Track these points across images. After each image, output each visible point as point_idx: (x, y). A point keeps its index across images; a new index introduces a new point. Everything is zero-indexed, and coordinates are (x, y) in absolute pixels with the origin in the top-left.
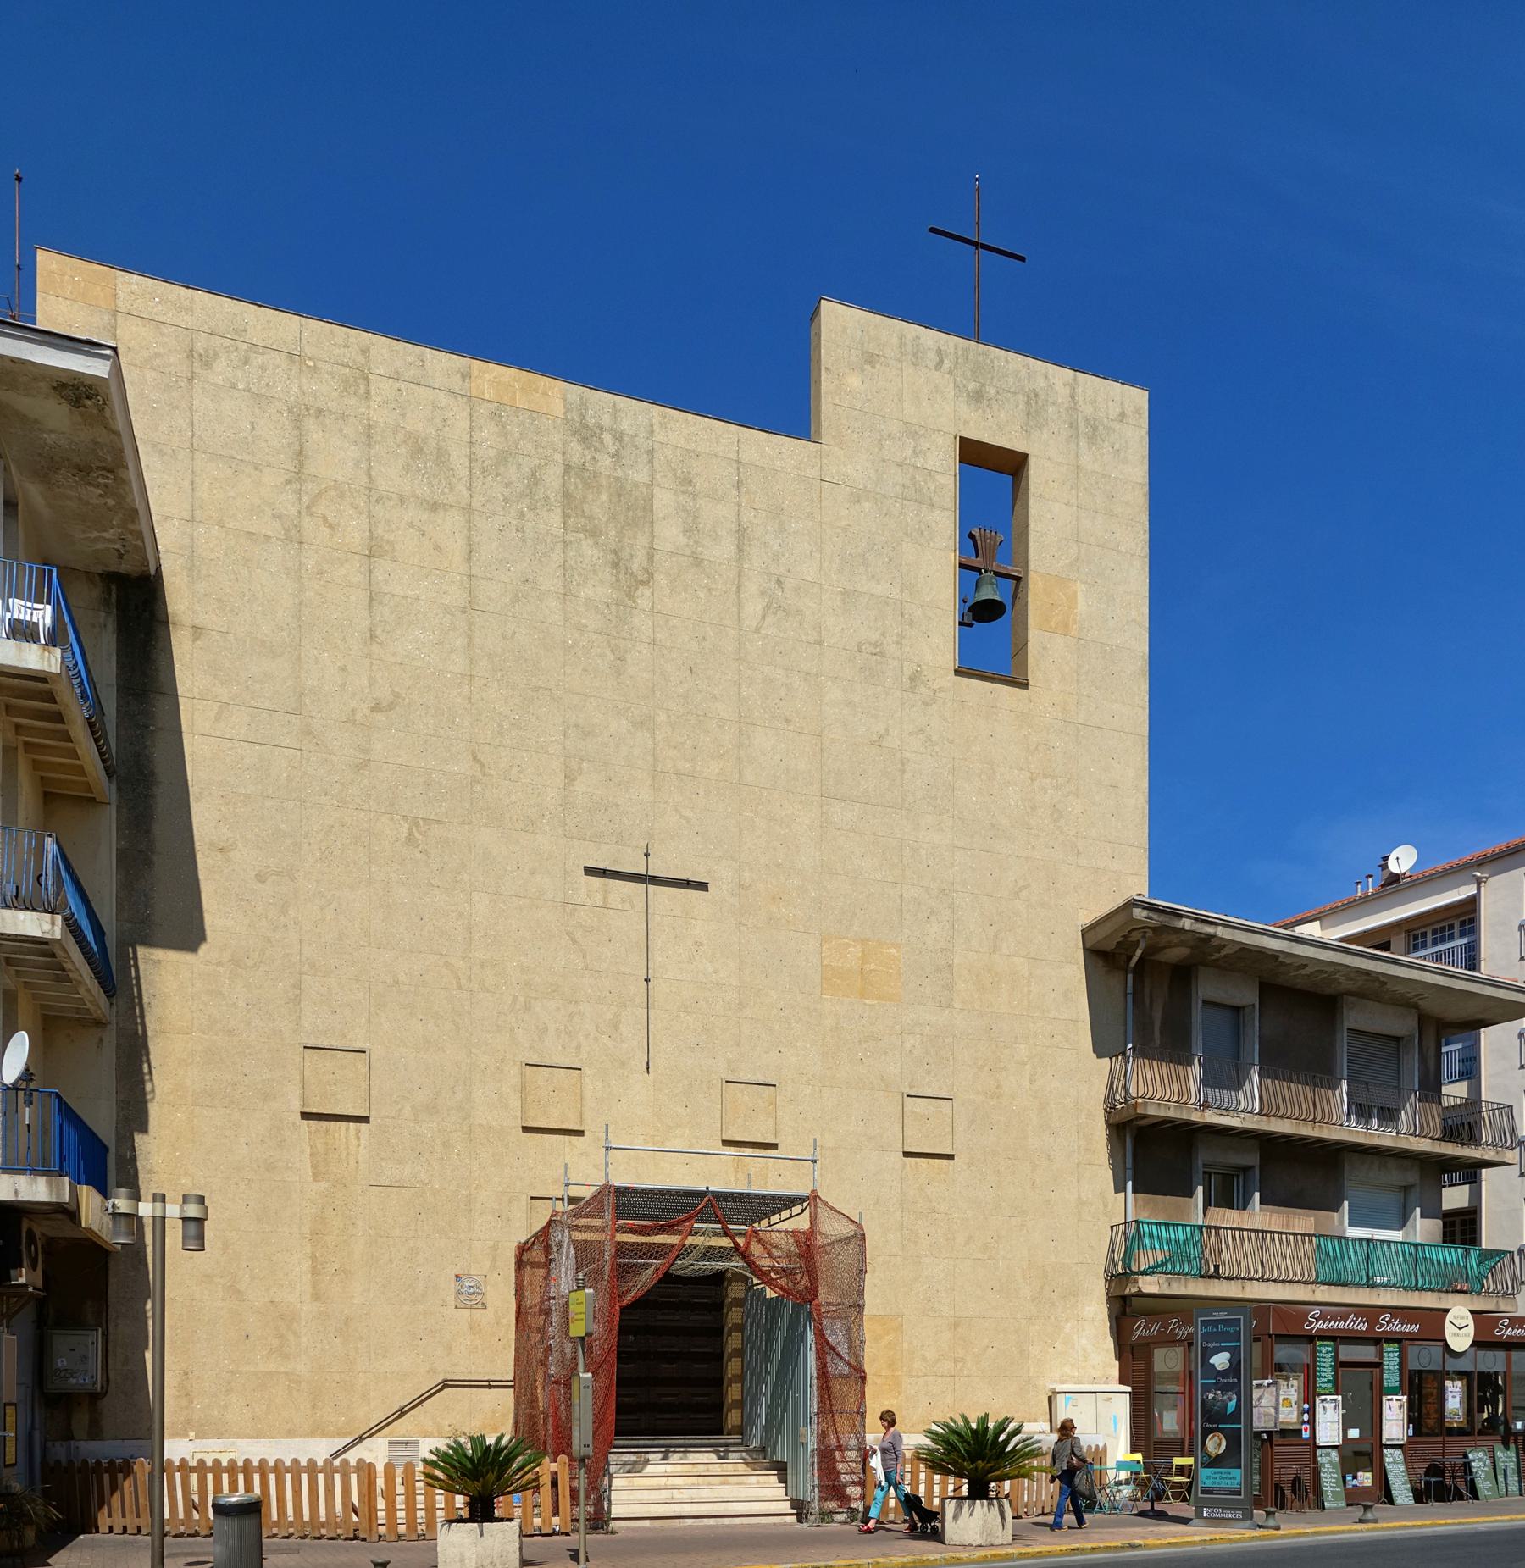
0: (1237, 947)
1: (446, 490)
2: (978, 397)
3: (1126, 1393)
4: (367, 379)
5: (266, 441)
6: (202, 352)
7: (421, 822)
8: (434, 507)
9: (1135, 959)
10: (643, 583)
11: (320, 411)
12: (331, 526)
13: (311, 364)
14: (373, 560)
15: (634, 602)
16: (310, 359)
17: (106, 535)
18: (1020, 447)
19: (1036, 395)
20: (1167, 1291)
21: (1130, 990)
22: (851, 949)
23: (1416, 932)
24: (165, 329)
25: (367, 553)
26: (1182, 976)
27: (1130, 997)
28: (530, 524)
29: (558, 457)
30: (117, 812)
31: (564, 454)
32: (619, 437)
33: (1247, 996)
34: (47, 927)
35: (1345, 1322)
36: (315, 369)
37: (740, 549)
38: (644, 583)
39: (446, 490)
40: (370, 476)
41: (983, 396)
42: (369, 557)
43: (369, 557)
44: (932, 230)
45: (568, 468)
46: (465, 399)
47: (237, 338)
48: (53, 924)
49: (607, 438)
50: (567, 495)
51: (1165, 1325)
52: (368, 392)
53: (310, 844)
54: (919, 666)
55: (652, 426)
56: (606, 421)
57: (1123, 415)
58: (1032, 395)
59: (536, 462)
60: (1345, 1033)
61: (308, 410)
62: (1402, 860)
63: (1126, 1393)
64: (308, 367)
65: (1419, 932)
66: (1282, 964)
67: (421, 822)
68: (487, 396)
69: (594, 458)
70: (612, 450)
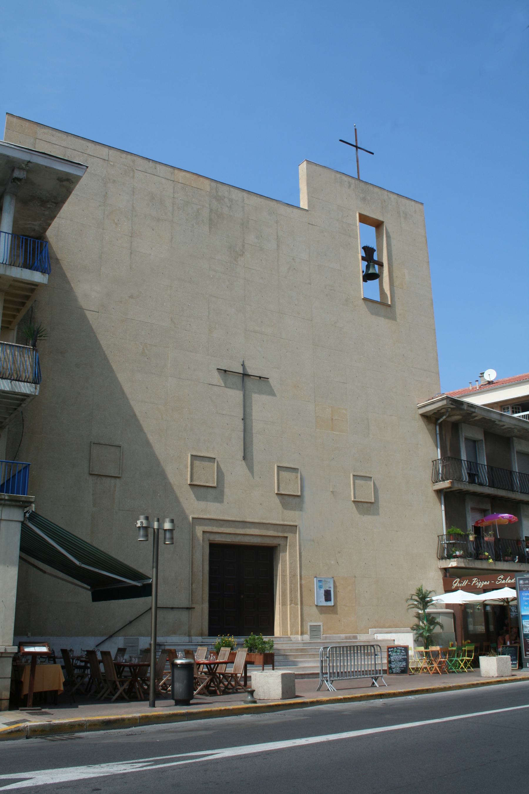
0: (481, 417)
1: (163, 214)
2: (364, 199)
3: (10, 657)
4: (133, 171)
5: (92, 190)
6: (69, 155)
7: (148, 346)
8: (158, 220)
9: (441, 420)
10: (240, 255)
11: (114, 181)
12: (116, 224)
13: (112, 164)
14: (132, 238)
15: (237, 262)
16: (112, 162)
17: (34, 223)
18: (381, 218)
19: (385, 201)
20: (467, 566)
21: (438, 432)
22: (328, 410)
23: (504, 407)
24: (55, 146)
25: (130, 235)
26: (455, 427)
27: (438, 436)
28: (196, 230)
29: (207, 206)
30: (17, 333)
31: (210, 205)
32: (231, 200)
33: (479, 436)
34: (33, 390)
35: (506, 580)
36: (113, 166)
37: (278, 246)
38: (242, 255)
39: (163, 214)
40: (133, 206)
41: (365, 199)
42: (131, 237)
43: (131, 237)
44: (341, 140)
45: (211, 210)
46: (172, 182)
47: (83, 151)
48: (36, 388)
49: (226, 200)
50: (210, 220)
51: (471, 581)
52: (133, 176)
53: (100, 352)
54: (348, 296)
55: (243, 198)
56: (226, 194)
57: (415, 211)
58: (383, 201)
59: (199, 207)
60: (515, 453)
61: (109, 180)
62: (490, 375)
63: (10, 657)
64: (111, 165)
65: (506, 407)
66: (496, 424)
67: (148, 346)
68: (180, 181)
69: (221, 207)
70: (229, 205)
